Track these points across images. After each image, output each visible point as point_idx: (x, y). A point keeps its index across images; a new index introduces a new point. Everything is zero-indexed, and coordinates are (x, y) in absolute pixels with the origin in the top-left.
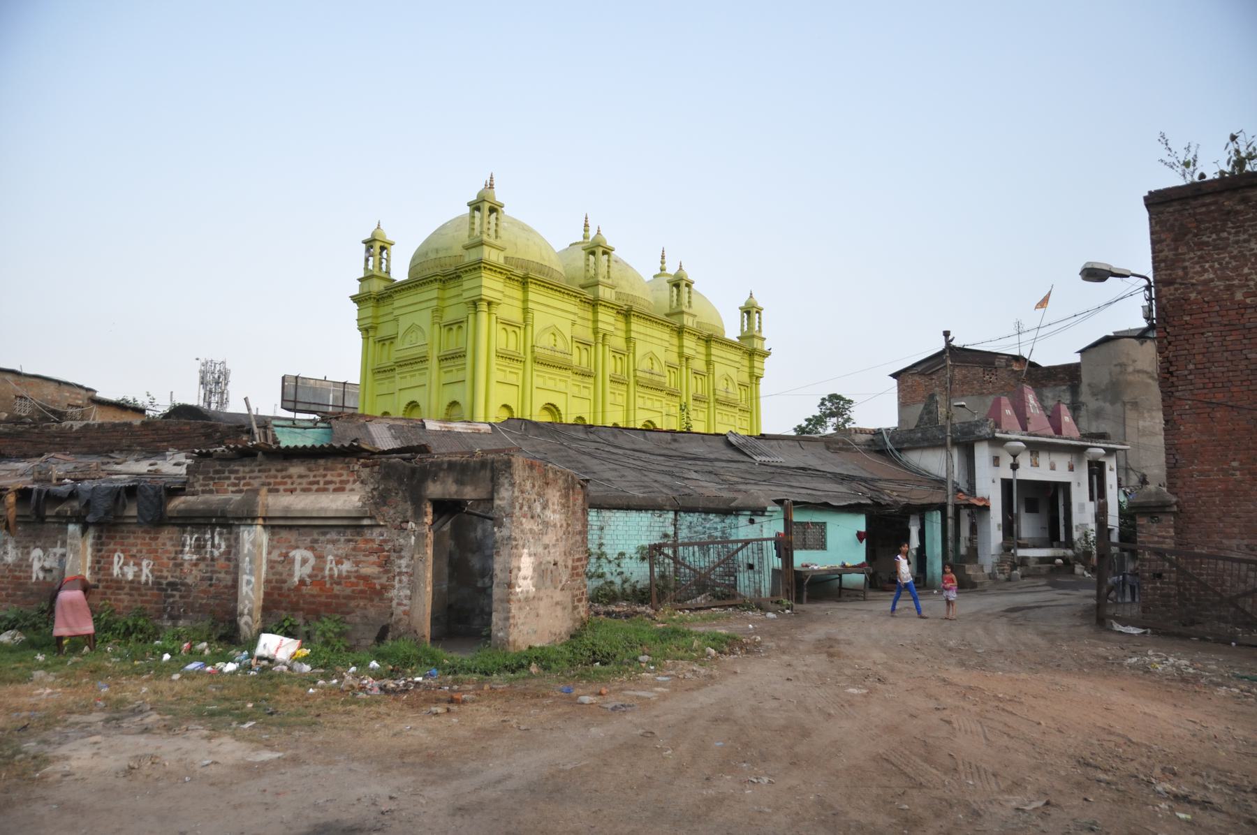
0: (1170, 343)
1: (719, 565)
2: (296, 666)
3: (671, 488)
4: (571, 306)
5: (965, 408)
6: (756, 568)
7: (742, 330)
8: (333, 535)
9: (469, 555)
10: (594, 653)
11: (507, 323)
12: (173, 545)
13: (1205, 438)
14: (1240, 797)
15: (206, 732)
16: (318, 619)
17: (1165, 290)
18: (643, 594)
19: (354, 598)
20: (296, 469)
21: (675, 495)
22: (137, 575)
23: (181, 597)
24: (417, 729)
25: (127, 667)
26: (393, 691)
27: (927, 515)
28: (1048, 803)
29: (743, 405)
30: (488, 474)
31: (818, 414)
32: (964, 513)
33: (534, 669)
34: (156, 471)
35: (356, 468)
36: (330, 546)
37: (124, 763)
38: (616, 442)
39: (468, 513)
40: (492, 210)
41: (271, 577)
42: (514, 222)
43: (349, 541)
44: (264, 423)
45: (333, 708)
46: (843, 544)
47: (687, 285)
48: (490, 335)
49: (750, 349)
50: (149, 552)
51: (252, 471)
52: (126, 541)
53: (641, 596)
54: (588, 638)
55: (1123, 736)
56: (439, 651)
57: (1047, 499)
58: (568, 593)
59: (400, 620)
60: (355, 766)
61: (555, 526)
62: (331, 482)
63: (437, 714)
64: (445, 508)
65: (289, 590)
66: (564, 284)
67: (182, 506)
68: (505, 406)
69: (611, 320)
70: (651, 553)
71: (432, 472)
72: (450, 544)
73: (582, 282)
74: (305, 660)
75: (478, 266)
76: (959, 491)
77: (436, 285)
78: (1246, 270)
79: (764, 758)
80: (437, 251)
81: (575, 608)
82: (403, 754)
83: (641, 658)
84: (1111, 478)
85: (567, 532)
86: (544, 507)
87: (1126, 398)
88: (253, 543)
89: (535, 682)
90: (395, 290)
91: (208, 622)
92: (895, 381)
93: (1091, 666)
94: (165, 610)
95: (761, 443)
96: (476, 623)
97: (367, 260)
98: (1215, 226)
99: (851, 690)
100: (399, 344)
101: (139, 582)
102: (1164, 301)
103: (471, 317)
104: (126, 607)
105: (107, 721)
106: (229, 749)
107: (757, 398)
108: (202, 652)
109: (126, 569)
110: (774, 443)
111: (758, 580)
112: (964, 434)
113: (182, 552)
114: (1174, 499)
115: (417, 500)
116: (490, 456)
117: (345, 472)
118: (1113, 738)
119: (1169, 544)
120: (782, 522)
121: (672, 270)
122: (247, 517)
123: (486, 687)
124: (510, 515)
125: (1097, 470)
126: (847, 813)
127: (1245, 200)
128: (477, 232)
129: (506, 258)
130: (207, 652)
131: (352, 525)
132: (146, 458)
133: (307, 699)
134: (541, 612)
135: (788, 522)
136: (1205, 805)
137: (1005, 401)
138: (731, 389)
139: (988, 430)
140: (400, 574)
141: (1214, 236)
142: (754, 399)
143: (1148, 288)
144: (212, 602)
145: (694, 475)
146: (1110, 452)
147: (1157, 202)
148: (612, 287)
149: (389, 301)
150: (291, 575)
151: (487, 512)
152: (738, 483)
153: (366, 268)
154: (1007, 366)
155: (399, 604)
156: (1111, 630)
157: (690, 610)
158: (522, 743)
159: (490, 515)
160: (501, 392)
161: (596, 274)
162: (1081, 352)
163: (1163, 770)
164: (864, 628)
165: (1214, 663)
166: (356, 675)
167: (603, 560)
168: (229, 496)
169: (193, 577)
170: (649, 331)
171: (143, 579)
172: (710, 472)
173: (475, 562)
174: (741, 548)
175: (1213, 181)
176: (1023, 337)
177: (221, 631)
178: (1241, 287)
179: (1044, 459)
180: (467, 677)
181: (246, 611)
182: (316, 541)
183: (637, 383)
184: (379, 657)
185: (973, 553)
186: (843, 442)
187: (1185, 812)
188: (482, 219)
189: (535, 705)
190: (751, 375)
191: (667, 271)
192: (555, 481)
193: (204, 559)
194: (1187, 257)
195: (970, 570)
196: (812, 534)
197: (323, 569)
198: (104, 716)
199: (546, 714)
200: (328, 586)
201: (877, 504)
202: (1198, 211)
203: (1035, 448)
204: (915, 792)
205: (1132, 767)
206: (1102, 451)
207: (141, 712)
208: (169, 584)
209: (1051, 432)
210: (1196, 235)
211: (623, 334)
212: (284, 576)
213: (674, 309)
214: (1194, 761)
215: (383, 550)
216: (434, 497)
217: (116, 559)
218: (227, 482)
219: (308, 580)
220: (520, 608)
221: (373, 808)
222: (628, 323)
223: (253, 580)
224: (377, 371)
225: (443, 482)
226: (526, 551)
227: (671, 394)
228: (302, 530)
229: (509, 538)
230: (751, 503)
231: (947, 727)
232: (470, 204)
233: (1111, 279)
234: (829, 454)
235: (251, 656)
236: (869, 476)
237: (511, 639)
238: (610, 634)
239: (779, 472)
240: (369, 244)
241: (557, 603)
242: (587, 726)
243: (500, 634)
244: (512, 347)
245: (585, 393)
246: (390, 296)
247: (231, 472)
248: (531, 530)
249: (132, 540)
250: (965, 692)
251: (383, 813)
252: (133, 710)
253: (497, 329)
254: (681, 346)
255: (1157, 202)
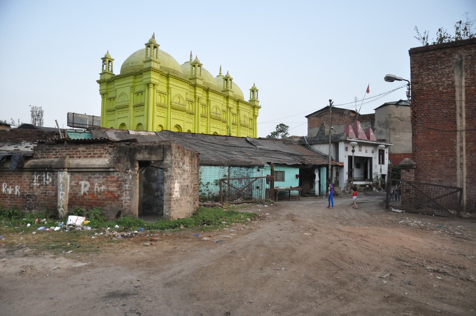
0: (415, 106)
1: (246, 187)
2: (85, 227)
3: (227, 157)
4: (186, 86)
5: (336, 129)
6: (260, 188)
7: (250, 98)
8: (97, 175)
9: (152, 183)
10: (204, 221)
11: (161, 93)
12: (29, 180)
13: (426, 141)
14: (455, 270)
15: (52, 256)
16: (92, 208)
17: (415, 86)
18: (217, 198)
19: (106, 200)
20: (81, 149)
21: (229, 160)
22: (13, 192)
23: (33, 200)
24: (141, 252)
25: (12, 229)
26: (127, 237)
27: (321, 169)
28: (391, 275)
29: (251, 127)
30: (162, 151)
31: (275, 131)
32: (334, 168)
33: (182, 227)
34: (18, 150)
35: (107, 148)
36: (96, 180)
37: (18, 269)
38: (204, 140)
39: (152, 166)
40: (155, 47)
41: (72, 192)
42: (163, 53)
43: (104, 177)
44: (64, 131)
45: (104, 244)
46: (290, 180)
47: (230, 80)
48: (154, 97)
49: (254, 105)
50: (18, 182)
51: (62, 149)
52: (8, 178)
53: (216, 199)
54: (200, 214)
55: (409, 249)
56: (142, 221)
57: (363, 164)
58: (192, 197)
59: (126, 209)
60: (118, 267)
61: (187, 171)
62: (96, 154)
63: (147, 246)
64: (144, 164)
65: (79, 197)
66: (183, 78)
67: (32, 163)
68: (160, 125)
69: (201, 93)
70: (219, 183)
71: (139, 149)
72: (144, 178)
73: (190, 77)
74: (88, 225)
75: (149, 70)
76: (333, 160)
77: (132, 77)
78: (444, 79)
79: (280, 260)
80: (132, 63)
81: (195, 203)
82: (137, 262)
83: (223, 222)
84: (386, 156)
85: (191, 174)
86: (183, 164)
87: (391, 127)
88: (64, 178)
89: (183, 232)
90: (115, 78)
91: (45, 211)
92: (307, 119)
93: (387, 223)
94: (26, 206)
95: (259, 141)
96: (155, 210)
97: (103, 66)
98: (434, 62)
99: (306, 234)
100: (117, 100)
101: (14, 195)
102: (414, 90)
103: (146, 90)
104: (9, 205)
105: (7, 252)
106: (63, 262)
107: (256, 124)
108: (44, 222)
109: (8, 189)
110: (264, 141)
111: (260, 193)
112: (335, 139)
113: (33, 182)
114: (415, 163)
115: (132, 161)
116: (162, 143)
117: (102, 150)
118: (405, 250)
119: (412, 180)
120: (270, 171)
121: (224, 74)
122: (61, 168)
123: (164, 235)
124: (170, 167)
125: (381, 153)
126: (318, 281)
127: (445, 53)
128: (149, 56)
129: (160, 67)
130: (46, 222)
131: (105, 171)
132: (13, 145)
133: (92, 241)
134: (182, 205)
135: (272, 170)
136: (445, 273)
137: (350, 126)
138: (246, 120)
139: (344, 137)
140: (126, 190)
141: (433, 66)
142: (255, 124)
143: (409, 85)
144: (46, 202)
145: (235, 153)
146: (387, 146)
147: (413, 52)
148: (202, 80)
149: (113, 83)
150: (80, 191)
151: (161, 166)
152: (251, 156)
153: (103, 69)
154: (348, 114)
155: (125, 202)
156: (391, 211)
157: (235, 204)
158: (189, 258)
159: (161, 166)
160: (157, 121)
161: (195, 75)
162: (375, 109)
163: (426, 261)
164: (306, 210)
165: (429, 223)
166: (110, 231)
167: (201, 185)
168: (53, 159)
169: (37, 193)
170: (216, 97)
171: (16, 193)
172: (241, 152)
173: (154, 185)
174: (255, 180)
175: (431, 46)
176: (357, 103)
177: (51, 214)
178: (442, 85)
179: (363, 148)
180: (155, 230)
181: (61, 206)
182: (90, 178)
183: (211, 117)
184: (118, 223)
185: (337, 183)
186: (288, 141)
187: (439, 276)
188: (151, 50)
189: (185, 241)
190: (254, 115)
191: (222, 74)
192: (187, 153)
193: (42, 185)
194: (423, 74)
195: (336, 189)
196: (279, 176)
197: (93, 189)
198: (5, 250)
199: (190, 245)
200: (96, 195)
201: (304, 165)
202: (428, 56)
203: (361, 144)
204: (340, 272)
205: (415, 260)
206: (384, 146)
207: (22, 248)
208: (28, 195)
209: (366, 138)
210: (427, 66)
211: (206, 98)
212: (77, 192)
213: (225, 89)
214: (435, 258)
215: (119, 181)
216: (139, 159)
217: (3, 185)
218: (51, 154)
219: (87, 193)
220: (175, 204)
221: (131, 285)
222: (208, 94)
223: (64, 193)
224: (107, 111)
225: (143, 154)
226: (177, 181)
227: (224, 122)
228: (84, 173)
229: (170, 176)
230: (258, 163)
231: (345, 247)
232: (146, 44)
233: (395, 81)
234: (284, 146)
235: (65, 224)
236: (300, 154)
237: (171, 216)
238: (208, 213)
239: (266, 152)
240: (104, 59)
241: (188, 202)
242: (208, 249)
243: (167, 214)
244: (163, 102)
245: (191, 121)
246: (113, 81)
247: (53, 149)
248: (178, 173)
249: (10, 178)
250: (349, 234)
251: (136, 287)
252: (18, 247)
253: (157, 95)
254: (228, 104)
255: (413, 52)
